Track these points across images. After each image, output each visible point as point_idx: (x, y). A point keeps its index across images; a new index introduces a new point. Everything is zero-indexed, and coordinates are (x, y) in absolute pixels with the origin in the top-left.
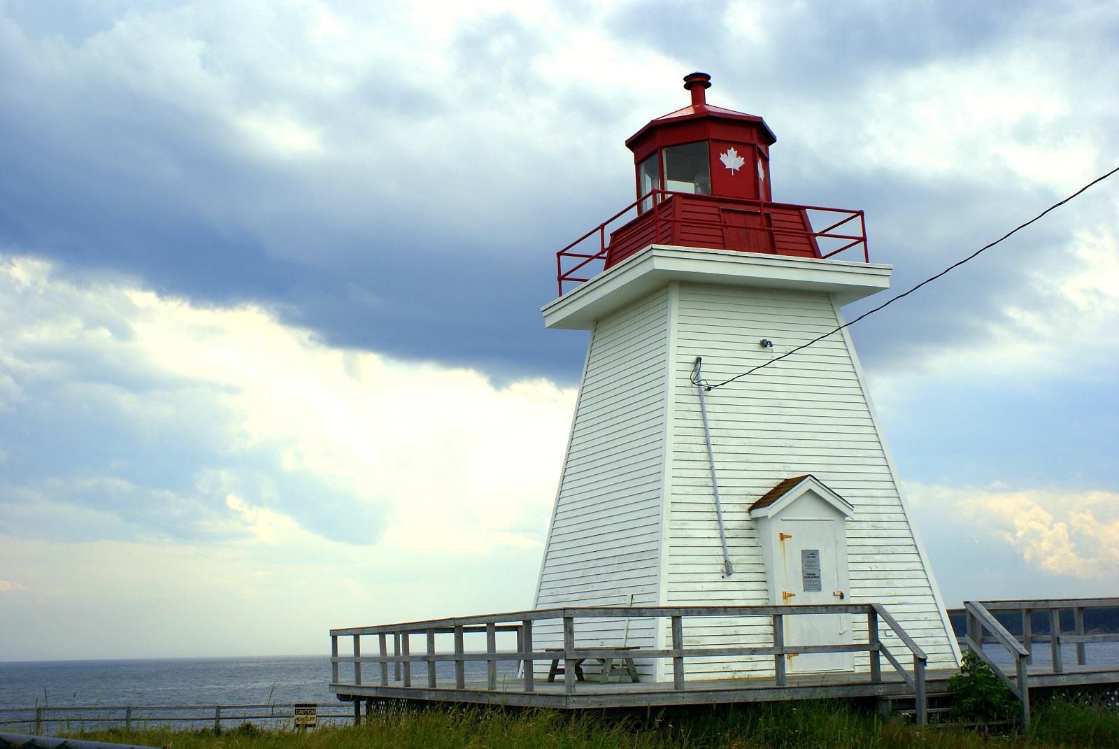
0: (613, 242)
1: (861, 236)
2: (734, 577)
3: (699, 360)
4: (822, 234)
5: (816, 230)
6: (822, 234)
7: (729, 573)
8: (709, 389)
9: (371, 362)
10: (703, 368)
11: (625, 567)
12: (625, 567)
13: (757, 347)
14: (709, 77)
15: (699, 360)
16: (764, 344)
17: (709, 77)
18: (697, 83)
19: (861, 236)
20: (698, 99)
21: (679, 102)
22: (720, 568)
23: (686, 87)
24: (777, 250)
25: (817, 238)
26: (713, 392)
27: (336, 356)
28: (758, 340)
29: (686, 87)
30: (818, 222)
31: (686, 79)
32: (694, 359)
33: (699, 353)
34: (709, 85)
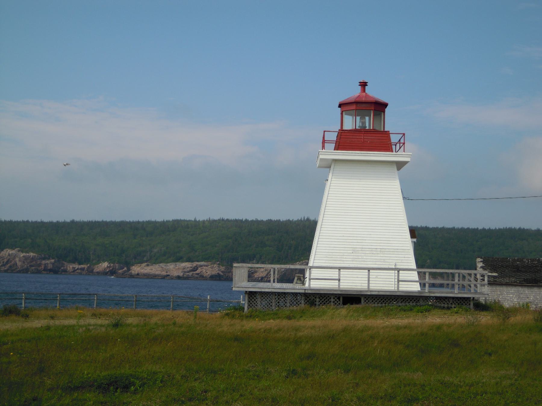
18: (364, 85)
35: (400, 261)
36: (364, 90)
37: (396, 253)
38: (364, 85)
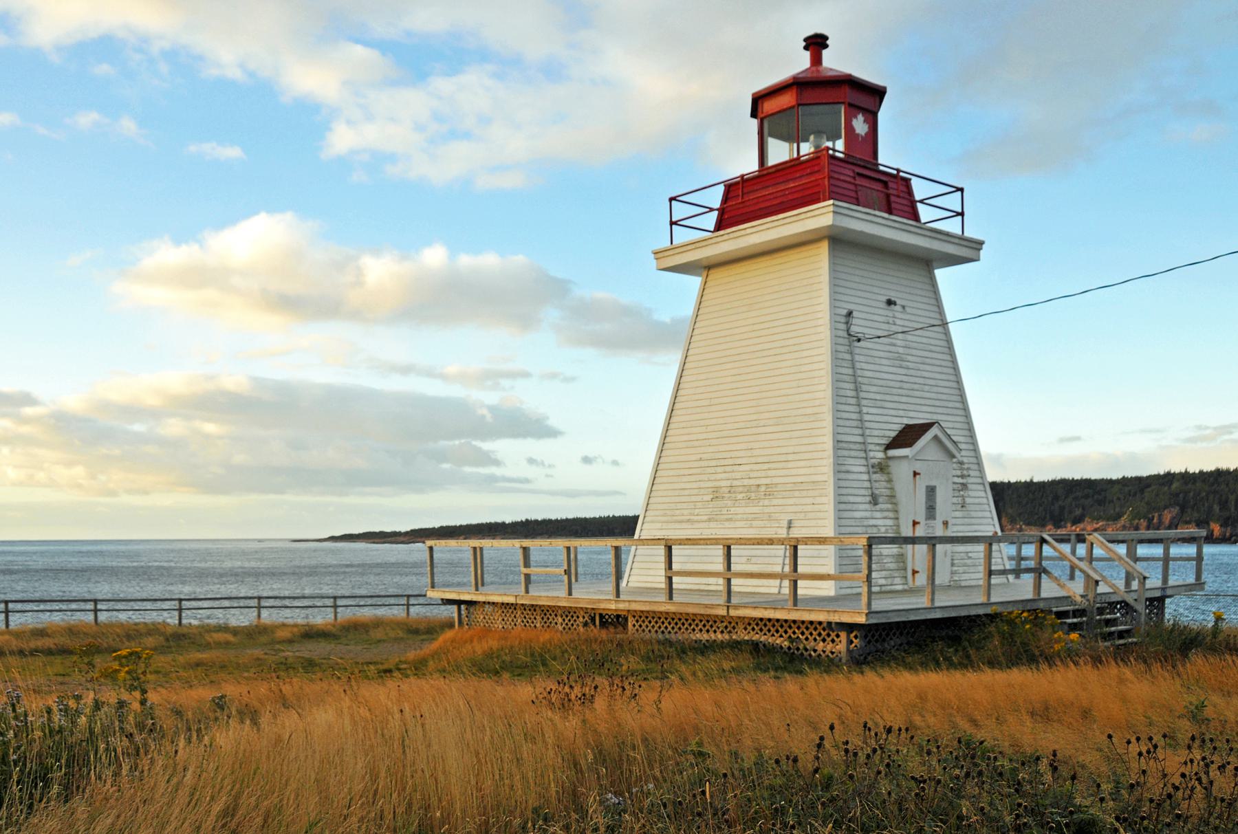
0: (725, 203)
1: (674, 226)
2: (878, 507)
3: (850, 314)
4: (921, 201)
5: (917, 197)
6: (921, 201)
7: (876, 504)
8: (859, 340)
9: (1058, 478)
10: (854, 321)
11: (721, 421)
12: (721, 421)
13: (884, 305)
14: (826, 38)
15: (850, 314)
16: (890, 303)
17: (826, 38)
18: (816, 43)
19: (674, 226)
20: (817, 60)
21: (801, 62)
22: (868, 499)
23: (806, 48)
24: (894, 212)
25: (919, 205)
26: (861, 344)
27: (1063, 477)
28: (884, 299)
29: (806, 48)
30: (920, 190)
31: (805, 40)
32: (845, 312)
33: (851, 307)
34: (826, 46)
35: (802, 516)
36: (817, 60)
37: (797, 494)
38: (816, 43)
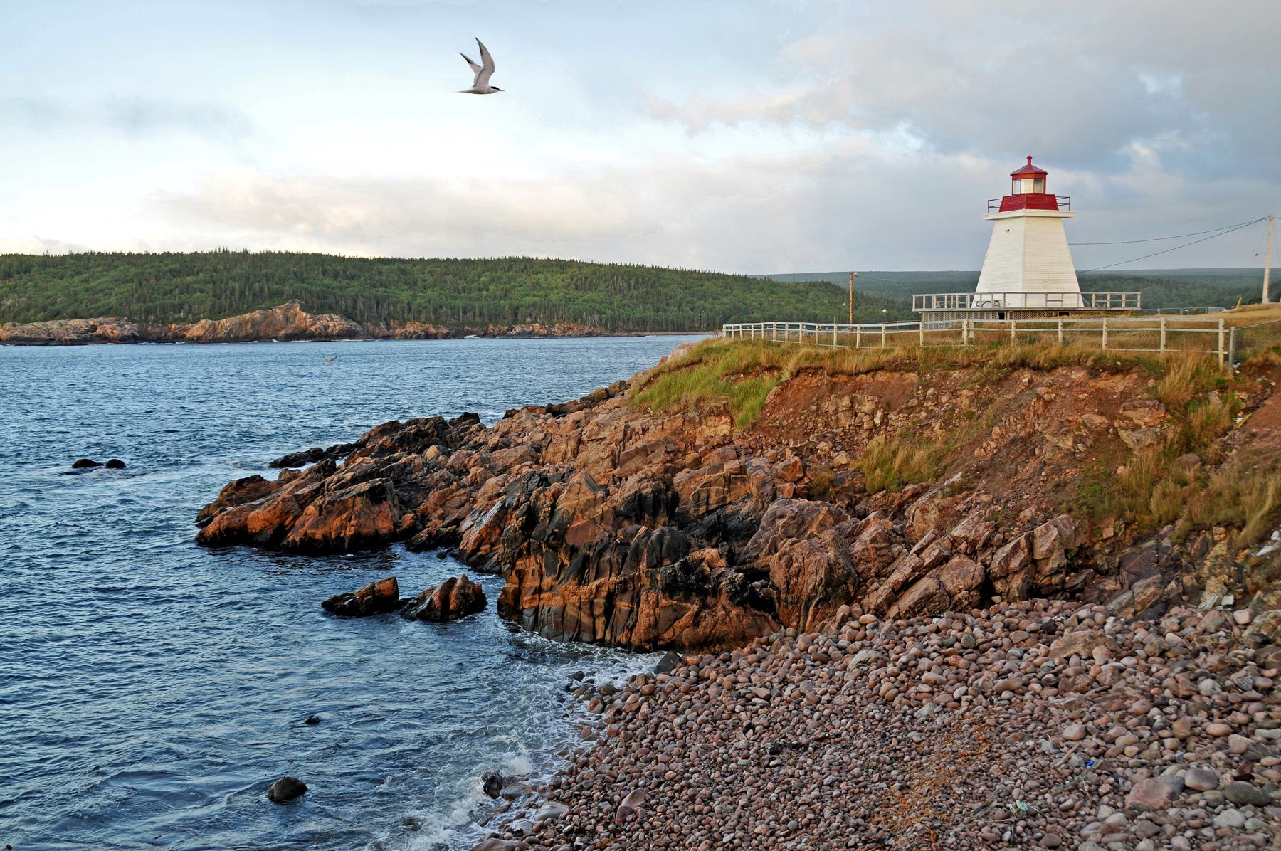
18: (1030, 158)
20: (1030, 162)
36: (1030, 162)
38: (1030, 158)
